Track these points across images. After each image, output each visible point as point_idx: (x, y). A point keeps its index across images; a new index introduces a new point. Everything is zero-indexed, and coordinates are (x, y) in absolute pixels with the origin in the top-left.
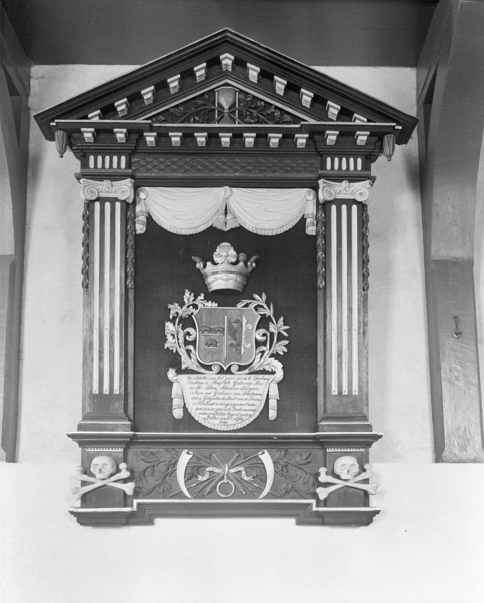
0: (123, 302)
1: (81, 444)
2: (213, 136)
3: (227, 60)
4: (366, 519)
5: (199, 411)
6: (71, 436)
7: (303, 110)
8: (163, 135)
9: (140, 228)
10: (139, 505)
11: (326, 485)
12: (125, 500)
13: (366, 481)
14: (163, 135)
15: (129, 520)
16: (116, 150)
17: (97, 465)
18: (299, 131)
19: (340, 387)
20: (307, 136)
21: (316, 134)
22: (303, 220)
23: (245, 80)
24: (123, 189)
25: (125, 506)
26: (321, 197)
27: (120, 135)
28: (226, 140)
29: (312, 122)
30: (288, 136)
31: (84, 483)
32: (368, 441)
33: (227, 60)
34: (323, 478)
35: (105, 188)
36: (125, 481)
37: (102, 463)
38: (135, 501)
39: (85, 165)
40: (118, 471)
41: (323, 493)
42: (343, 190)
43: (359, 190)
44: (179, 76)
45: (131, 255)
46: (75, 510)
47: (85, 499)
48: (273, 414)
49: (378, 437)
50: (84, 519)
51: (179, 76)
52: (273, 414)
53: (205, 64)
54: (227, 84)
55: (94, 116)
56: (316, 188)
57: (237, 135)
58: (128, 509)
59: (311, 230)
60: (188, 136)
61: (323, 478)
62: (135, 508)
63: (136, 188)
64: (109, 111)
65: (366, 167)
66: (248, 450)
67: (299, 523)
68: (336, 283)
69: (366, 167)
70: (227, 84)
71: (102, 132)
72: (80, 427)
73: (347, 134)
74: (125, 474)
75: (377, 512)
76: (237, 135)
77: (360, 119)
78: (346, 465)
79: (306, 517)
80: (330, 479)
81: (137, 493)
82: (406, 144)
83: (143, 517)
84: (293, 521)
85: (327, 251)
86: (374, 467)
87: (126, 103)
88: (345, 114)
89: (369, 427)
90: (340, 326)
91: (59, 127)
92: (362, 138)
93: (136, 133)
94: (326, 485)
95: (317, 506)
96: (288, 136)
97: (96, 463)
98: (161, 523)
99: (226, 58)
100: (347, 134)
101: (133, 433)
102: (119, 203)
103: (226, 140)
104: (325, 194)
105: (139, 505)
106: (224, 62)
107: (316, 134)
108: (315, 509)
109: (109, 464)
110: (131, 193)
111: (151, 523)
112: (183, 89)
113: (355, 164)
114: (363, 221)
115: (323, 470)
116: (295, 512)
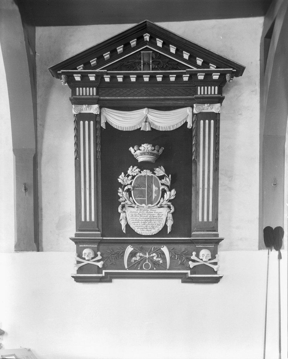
0: (96, 201)
1: (76, 243)
2: (140, 77)
3: (147, 37)
4: (217, 280)
5: (132, 221)
6: (73, 277)
7: (185, 60)
8: (113, 77)
9: (103, 125)
10: (105, 273)
11: (194, 261)
12: (99, 270)
13: (216, 264)
14: (113, 77)
15: (101, 280)
16: (91, 85)
17: (85, 253)
18: (185, 73)
19: (204, 89)
20: (189, 75)
21: (193, 75)
22: (186, 123)
23: (155, 45)
24: (94, 109)
25: (99, 273)
26: (195, 111)
27: (92, 78)
28: (146, 79)
29: (195, 69)
30: (179, 77)
31: (78, 262)
32: (217, 242)
33: (147, 37)
34: (193, 257)
35: (86, 109)
36: (98, 261)
37: (87, 252)
38: (104, 271)
39: (74, 93)
40: (96, 255)
41: (192, 265)
42: (207, 108)
43: (215, 108)
44: (123, 46)
45: (99, 141)
46: (74, 275)
47: (80, 270)
48: (169, 230)
49: (222, 239)
50: (77, 279)
51: (123, 46)
52: (169, 230)
53: (136, 39)
54: (147, 49)
55: (80, 68)
56: (193, 107)
57: (153, 77)
58: (100, 275)
59: (189, 125)
60: (126, 77)
61: (193, 257)
62: (103, 274)
63: (100, 108)
64: (87, 65)
65: (220, 92)
66: (156, 246)
67: (183, 282)
68: (202, 149)
69: (220, 92)
70: (147, 49)
71: (84, 76)
72: (76, 235)
73: (208, 75)
74: (99, 257)
75: (221, 277)
76: (153, 77)
77: (213, 67)
78: (205, 254)
79: (186, 280)
80: (196, 259)
81: (104, 267)
82: (241, 76)
83: (107, 279)
84: (180, 280)
85: (197, 135)
86: (221, 254)
87: (96, 60)
88: (206, 64)
89: (217, 235)
90: (204, 171)
91: (63, 73)
92: (216, 77)
93: (99, 77)
94: (194, 261)
95: (191, 274)
96: (179, 77)
97: (85, 252)
98: (115, 281)
99: (146, 35)
100: (208, 75)
101: (101, 238)
102: (92, 122)
103: (146, 79)
104: (197, 109)
105: (105, 273)
106: (145, 37)
107: (193, 75)
108: (190, 276)
109: (91, 253)
110: (98, 110)
111: (110, 281)
112: (125, 52)
113: (213, 91)
114: (216, 136)
115: (194, 253)
116: (181, 276)
